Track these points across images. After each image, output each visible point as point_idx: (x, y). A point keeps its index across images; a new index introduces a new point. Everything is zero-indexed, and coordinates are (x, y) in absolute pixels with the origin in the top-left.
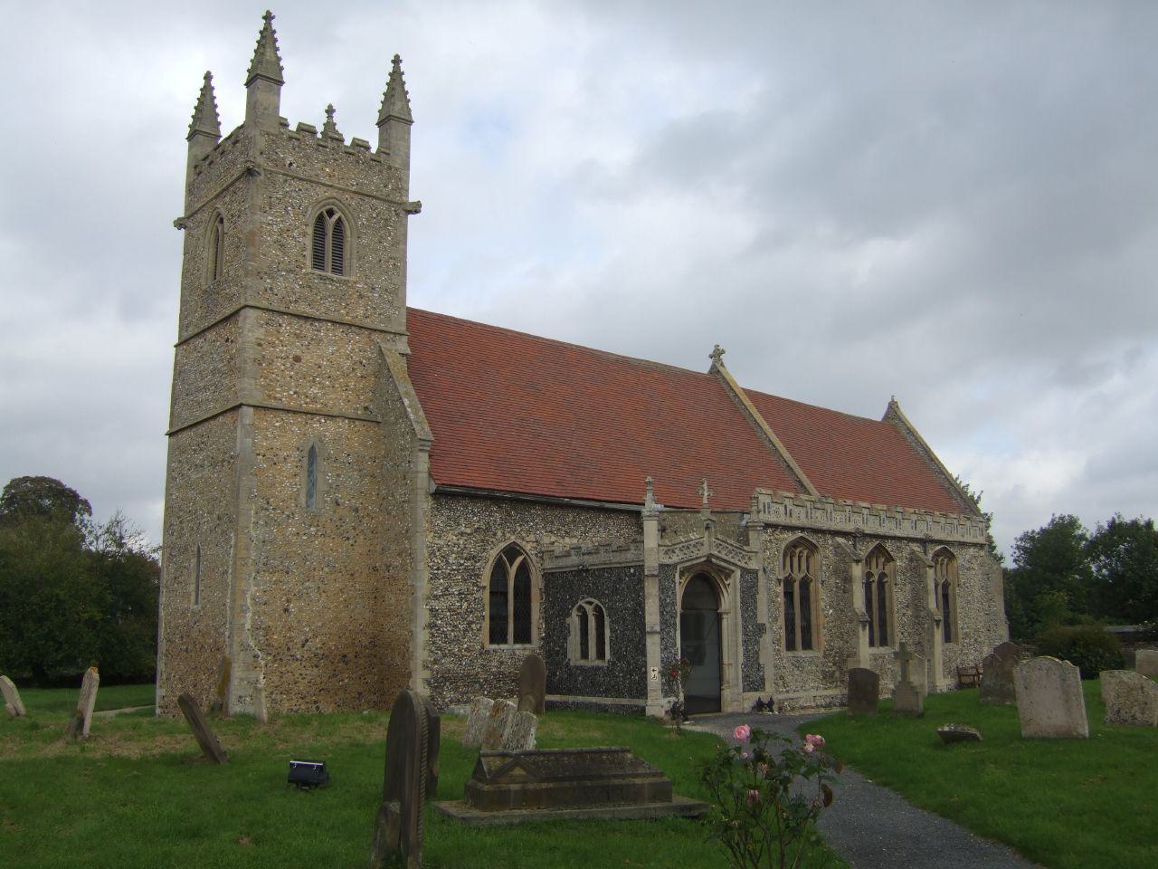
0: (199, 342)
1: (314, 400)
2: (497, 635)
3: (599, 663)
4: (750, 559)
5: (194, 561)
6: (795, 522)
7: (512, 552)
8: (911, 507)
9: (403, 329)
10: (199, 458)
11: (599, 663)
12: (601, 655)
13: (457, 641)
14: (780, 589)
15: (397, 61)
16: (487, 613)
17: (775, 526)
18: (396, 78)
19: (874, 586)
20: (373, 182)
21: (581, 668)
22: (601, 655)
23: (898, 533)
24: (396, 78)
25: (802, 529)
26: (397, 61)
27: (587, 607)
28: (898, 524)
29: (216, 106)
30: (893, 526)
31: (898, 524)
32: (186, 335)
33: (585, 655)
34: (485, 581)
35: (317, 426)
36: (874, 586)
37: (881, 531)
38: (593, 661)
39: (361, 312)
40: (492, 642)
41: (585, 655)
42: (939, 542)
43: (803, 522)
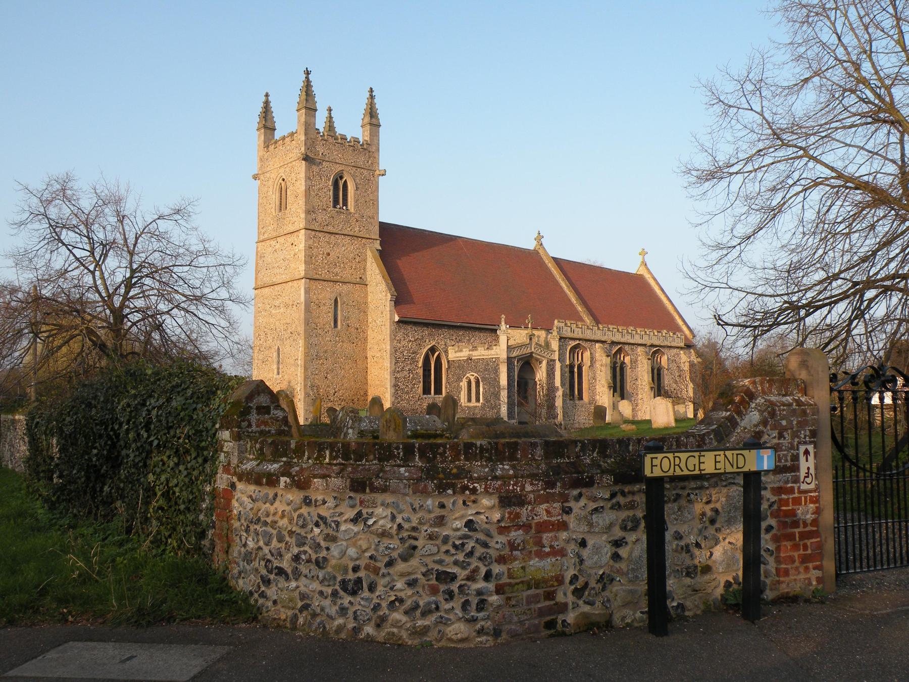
0: (273, 243)
1: (337, 275)
2: (426, 391)
3: (477, 404)
5: (275, 354)
6: (575, 336)
7: (433, 350)
8: (612, 324)
9: (377, 237)
10: (277, 303)
11: (477, 404)
12: (478, 400)
13: (407, 393)
14: (567, 370)
15: (267, 95)
16: (421, 380)
18: (267, 104)
19: (618, 369)
20: (361, 160)
21: (468, 407)
22: (478, 400)
23: (632, 342)
24: (267, 104)
25: (580, 339)
26: (267, 95)
27: (472, 378)
28: (632, 336)
30: (629, 337)
31: (632, 336)
32: (262, 238)
33: (469, 400)
34: (420, 364)
35: (339, 287)
36: (618, 369)
37: (623, 340)
38: (474, 403)
39: (357, 229)
40: (424, 394)
41: (469, 400)
42: (656, 346)
43: (580, 336)
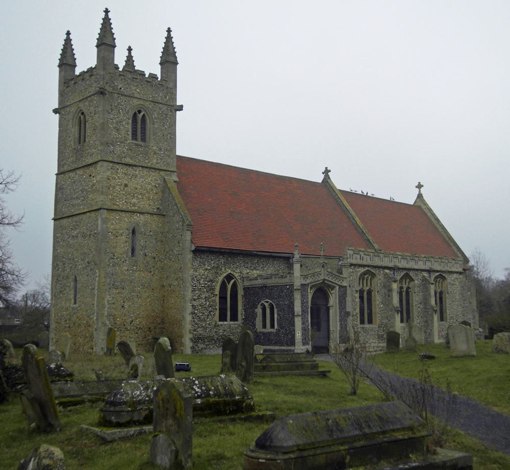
4: (343, 281)
6: (365, 263)
17: (355, 265)
26: (169, 31)
29: (101, 29)
